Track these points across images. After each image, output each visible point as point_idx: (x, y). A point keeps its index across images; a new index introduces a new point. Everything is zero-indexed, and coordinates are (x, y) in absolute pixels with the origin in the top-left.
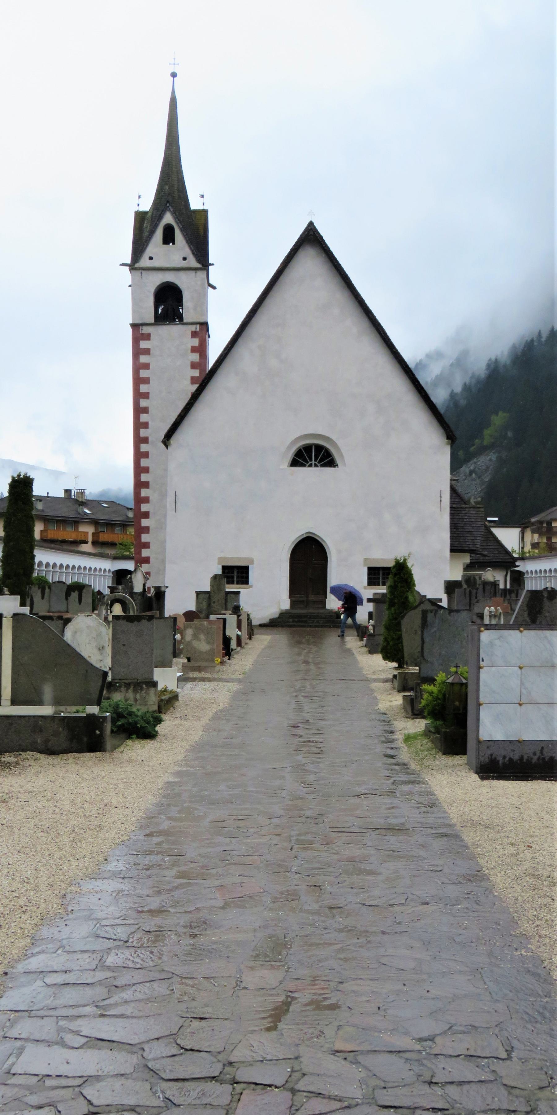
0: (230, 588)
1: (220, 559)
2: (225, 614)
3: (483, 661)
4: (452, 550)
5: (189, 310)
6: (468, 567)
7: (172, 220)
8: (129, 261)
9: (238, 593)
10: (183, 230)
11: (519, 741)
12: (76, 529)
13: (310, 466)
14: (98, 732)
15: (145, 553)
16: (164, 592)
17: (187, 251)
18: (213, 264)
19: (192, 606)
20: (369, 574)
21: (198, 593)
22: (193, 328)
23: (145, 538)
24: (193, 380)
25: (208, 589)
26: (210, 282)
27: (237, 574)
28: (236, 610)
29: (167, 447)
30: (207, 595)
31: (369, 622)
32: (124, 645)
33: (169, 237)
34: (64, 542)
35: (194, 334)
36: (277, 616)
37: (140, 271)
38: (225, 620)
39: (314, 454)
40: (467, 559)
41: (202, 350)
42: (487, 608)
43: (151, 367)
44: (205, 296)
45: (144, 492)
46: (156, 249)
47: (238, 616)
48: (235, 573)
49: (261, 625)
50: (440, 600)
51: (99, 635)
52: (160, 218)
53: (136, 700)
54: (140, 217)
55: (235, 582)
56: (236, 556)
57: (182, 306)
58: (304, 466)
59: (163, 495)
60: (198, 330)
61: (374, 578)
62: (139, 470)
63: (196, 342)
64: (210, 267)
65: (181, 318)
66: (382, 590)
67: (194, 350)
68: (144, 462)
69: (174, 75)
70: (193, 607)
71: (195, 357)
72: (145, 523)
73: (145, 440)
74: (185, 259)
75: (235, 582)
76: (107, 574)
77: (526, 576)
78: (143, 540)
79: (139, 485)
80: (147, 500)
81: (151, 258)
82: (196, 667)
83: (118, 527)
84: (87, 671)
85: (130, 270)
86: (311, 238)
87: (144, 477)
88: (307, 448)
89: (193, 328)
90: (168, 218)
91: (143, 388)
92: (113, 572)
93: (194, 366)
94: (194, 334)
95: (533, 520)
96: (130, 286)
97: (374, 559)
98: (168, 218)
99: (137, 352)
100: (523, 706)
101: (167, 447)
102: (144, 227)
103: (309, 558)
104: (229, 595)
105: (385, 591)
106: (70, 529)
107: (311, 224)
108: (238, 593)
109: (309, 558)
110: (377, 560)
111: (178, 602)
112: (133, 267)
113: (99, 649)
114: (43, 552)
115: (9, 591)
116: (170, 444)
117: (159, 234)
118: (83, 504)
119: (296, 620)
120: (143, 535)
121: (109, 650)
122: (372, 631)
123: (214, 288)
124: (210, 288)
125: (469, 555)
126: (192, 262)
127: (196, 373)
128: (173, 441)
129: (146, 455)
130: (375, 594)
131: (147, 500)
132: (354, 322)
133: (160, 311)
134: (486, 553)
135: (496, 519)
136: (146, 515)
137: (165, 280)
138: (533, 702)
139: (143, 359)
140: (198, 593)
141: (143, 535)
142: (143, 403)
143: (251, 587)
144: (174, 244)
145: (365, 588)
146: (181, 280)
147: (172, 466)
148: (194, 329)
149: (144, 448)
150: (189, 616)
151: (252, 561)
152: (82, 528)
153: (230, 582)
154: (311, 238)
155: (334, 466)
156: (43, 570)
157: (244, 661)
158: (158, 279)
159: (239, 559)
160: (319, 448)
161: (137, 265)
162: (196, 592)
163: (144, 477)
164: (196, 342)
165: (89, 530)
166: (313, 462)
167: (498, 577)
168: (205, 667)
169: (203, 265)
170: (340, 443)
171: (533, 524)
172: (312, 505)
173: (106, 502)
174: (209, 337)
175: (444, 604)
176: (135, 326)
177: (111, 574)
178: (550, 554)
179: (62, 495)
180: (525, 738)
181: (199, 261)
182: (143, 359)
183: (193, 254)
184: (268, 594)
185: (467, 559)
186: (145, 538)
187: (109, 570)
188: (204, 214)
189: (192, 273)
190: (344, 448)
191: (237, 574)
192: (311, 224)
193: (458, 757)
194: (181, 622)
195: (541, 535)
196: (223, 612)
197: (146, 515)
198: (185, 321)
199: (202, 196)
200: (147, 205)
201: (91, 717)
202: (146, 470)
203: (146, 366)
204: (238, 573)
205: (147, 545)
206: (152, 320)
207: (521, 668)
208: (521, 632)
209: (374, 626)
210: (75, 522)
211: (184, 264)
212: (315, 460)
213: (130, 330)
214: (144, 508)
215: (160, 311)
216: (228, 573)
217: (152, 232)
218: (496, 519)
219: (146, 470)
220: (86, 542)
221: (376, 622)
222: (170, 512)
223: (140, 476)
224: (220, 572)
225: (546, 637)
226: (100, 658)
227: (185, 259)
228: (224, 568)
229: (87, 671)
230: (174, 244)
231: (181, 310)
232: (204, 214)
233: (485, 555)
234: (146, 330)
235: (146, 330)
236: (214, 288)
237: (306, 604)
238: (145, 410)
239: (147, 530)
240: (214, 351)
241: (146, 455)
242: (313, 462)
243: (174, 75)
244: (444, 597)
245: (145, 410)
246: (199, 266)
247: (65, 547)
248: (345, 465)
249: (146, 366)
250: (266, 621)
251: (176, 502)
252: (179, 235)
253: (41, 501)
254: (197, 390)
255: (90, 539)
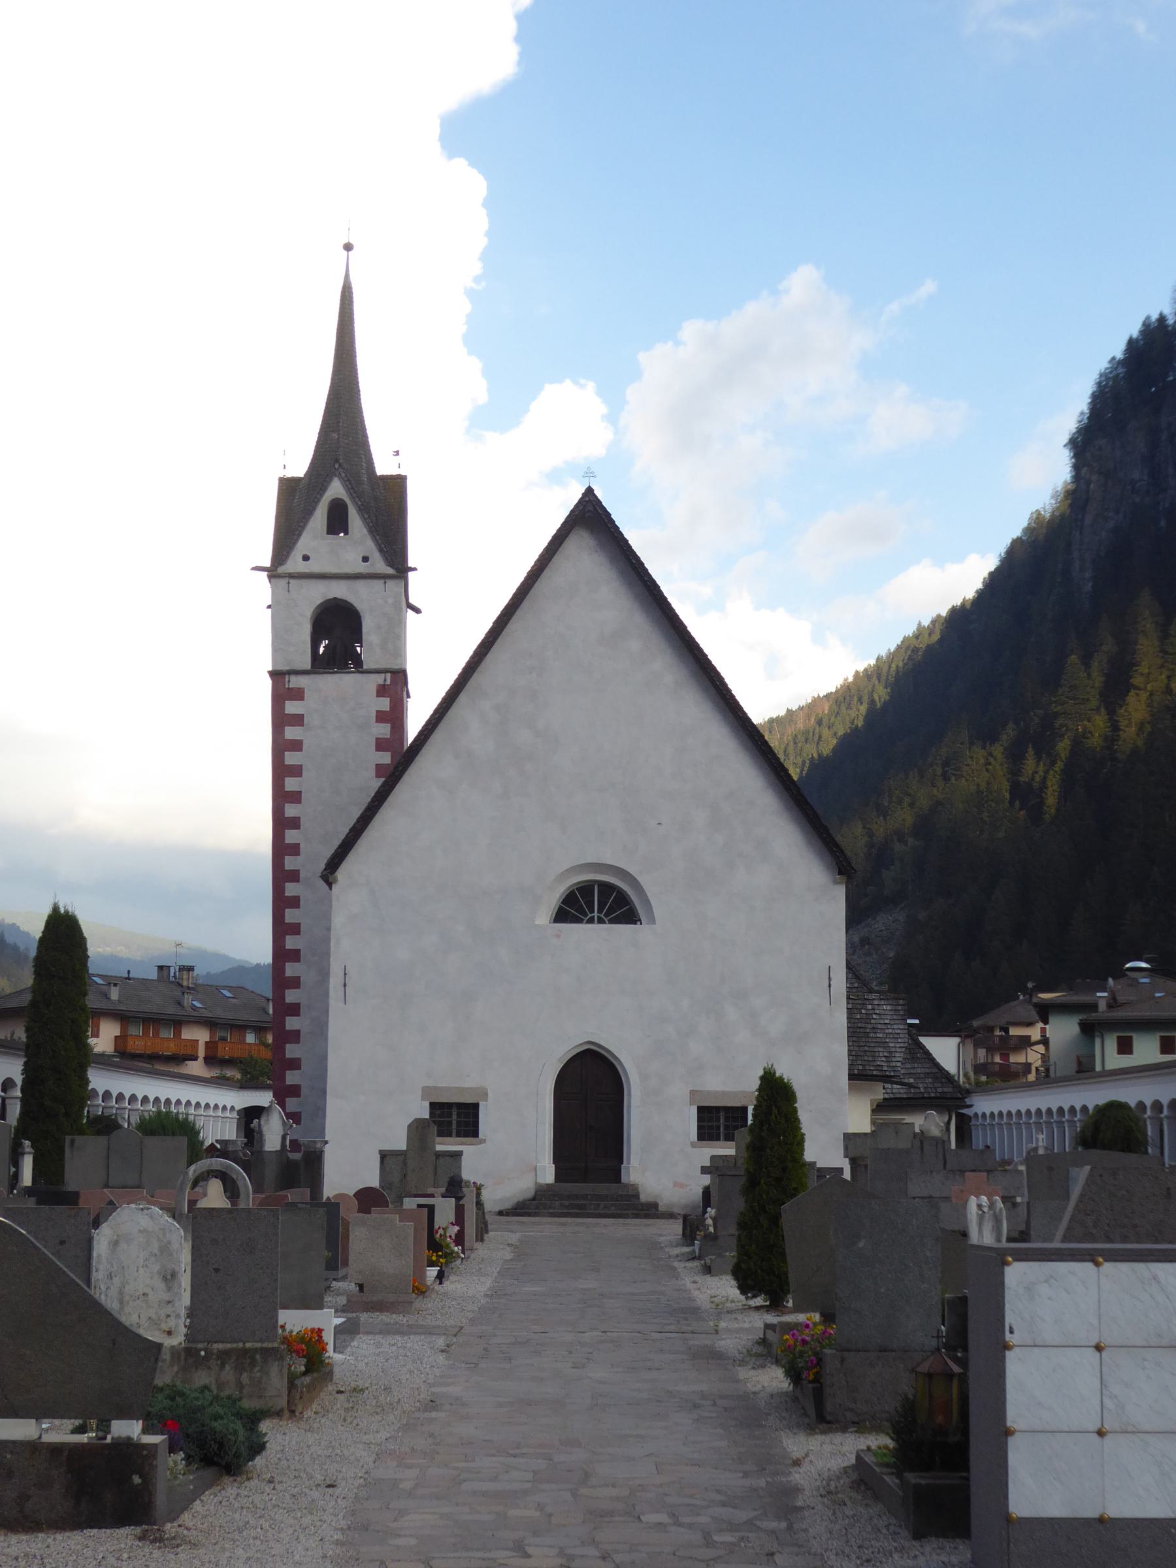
0: (444, 1145)
1: (426, 1091)
2: (432, 1196)
3: (1011, 1332)
4: (852, 1077)
5: (370, 651)
6: (879, 1108)
7: (345, 503)
8: (267, 563)
9: (459, 1154)
10: (362, 510)
11: (1101, 1520)
12: (178, 1034)
13: (591, 921)
14: (137, 1480)
15: (291, 1078)
16: (322, 1152)
17: (369, 546)
18: (414, 569)
19: (372, 1179)
20: (700, 1119)
21: (384, 1156)
22: (379, 679)
23: (291, 1051)
24: (379, 768)
25: (403, 1146)
26: (411, 601)
27: (457, 1117)
28: (455, 1187)
29: (330, 885)
30: (401, 1158)
31: (705, 1212)
32: (217, 1270)
33: (337, 522)
34: (154, 1058)
35: (382, 691)
36: (531, 1194)
37: (287, 580)
38: (431, 1209)
39: (600, 900)
40: (879, 1092)
41: (395, 716)
42: (973, 1198)
43: (305, 747)
44: (401, 623)
45: (291, 970)
46: (313, 535)
47: (458, 1199)
48: (454, 1117)
49: (500, 1213)
50: (841, 1170)
51: (165, 1249)
52: (323, 489)
53: (240, 1386)
54: (288, 487)
55: (454, 1131)
56: (457, 1081)
57: (360, 641)
58: (579, 921)
59: (324, 974)
60: (388, 682)
61: (711, 1128)
62: (282, 929)
63: (385, 704)
64: (411, 574)
65: (358, 662)
66: (727, 1150)
67: (381, 717)
68: (291, 916)
69: (348, 247)
70: (374, 1181)
71: (384, 730)
72: (291, 1023)
73: (294, 876)
74: (365, 559)
75: (454, 1131)
76: (228, 1114)
77: (973, 1122)
78: (288, 1055)
79: (282, 955)
80: (295, 983)
81: (306, 558)
82: (372, 1301)
83: (262, 1030)
84: (114, 1342)
85: (270, 577)
86: (590, 518)
87: (291, 942)
88: (585, 889)
89: (379, 679)
90: (336, 489)
91: (291, 784)
92: (239, 1112)
93: (381, 745)
94: (382, 691)
95: (976, 1023)
96: (269, 607)
97: (708, 1092)
98: (336, 489)
99: (281, 720)
100: (1108, 1439)
101: (330, 885)
102: (295, 501)
103: (590, 1094)
104: (441, 1160)
105: (732, 1152)
106: (167, 1033)
107: (589, 491)
108: (459, 1154)
109: (590, 1094)
110: (716, 1094)
111: (348, 1169)
112: (274, 572)
113: (165, 1279)
114: (108, 1074)
115: (32, 1147)
116: (336, 881)
117: (320, 517)
118: (192, 990)
119: (567, 1203)
120: (288, 1046)
121: (185, 1281)
122: (711, 1229)
123: (417, 611)
124: (410, 612)
125: (881, 1084)
126: (379, 565)
127: (386, 758)
128: (341, 874)
129: (295, 902)
130: (713, 1158)
131: (295, 983)
132: (664, 665)
133: (322, 650)
134: (912, 1080)
135: (917, 1022)
136: (294, 1010)
137: (331, 596)
138: (1130, 1429)
139: (291, 733)
140: (384, 1156)
141: (288, 1046)
142: (291, 811)
143: (484, 1141)
144: (346, 533)
145: (693, 1145)
146: (360, 596)
147: (338, 920)
148: (381, 682)
149: (291, 889)
150: (367, 1199)
151: (485, 1095)
152: (188, 1034)
153: (444, 1132)
154: (590, 518)
155: (635, 923)
156: (98, 1106)
157: (468, 1285)
158: (317, 594)
159: (462, 1090)
160: (607, 889)
161: (281, 570)
162: (381, 1152)
163: (291, 942)
164: (385, 704)
165: (201, 1036)
166: (596, 914)
167: (928, 1122)
168: (392, 1303)
169: (397, 570)
170: (643, 880)
171: (976, 1031)
172: (599, 991)
173: (229, 988)
174: (408, 696)
175: (847, 1175)
176: (275, 675)
177: (235, 1115)
178: (1003, 1084)
179: (153, 975)
180: (1115, 1510)
181: (390, 563)
182: (291, 733)
183: (381, 551)
184: (515, 1150)
185: (879, 1092)
186: (291, 1051)
187: (232, 1108)
188: (397, 485)
189: (378, 584)
190: (656, 889)
191: (457, 1117)
192: (589, 491)
193: (948, 1544)
194: (349, 1212)
195: (990, 1050)
196: (430, 1190)
197: (294, 1010)
198: (365, 667)
199: (397, 453)
200: (299, 468)
201: (126, 1446)
202: (295, 929)
203: (297, 746)
204: (459, 1115)
205: (295, 1064)
206: (307, 665)
207: (1099, 1348)
208: (1097, 1264)
209: (714, 1219)
210: (178, 1023)
211: (363, 568)
212: (600, 911)
213: (268, 683)
214: (291, 996)
215: (322, 650)
216: (439, 1116)
217: (309, 512)
218: (917, 1022)
219: (295, 929)
220: (196, 1059)
221: (718, 1210)
222: (335, 1003)
223: (284, 941)
224: (426, 1115)
225: (1155, 1278)
226: (166, 1296)
227: (365, 559)
228: (433, 1106)
229: (114, 1342)
230: (346, 533)
231: (358, 649)
232: (397, 485)
233: (910, 1085)
234: (295, 682)
235: (295, 682)
236: (417, 611)
237: (583, 1176)
238: (295, 823)
239: (295, 1036)
240: (415, 720)
241: (295, 902)
242: (596, 914)
243: (348, 247)
244: (846, 1165)
245: (295, 823)
246: (390, 571)
247: (159, 1067)
248: (652, 920)
249: (297, 746)
250: (507, 1205)
251: (345, 985)
252: (355, 520)
253: (115, 985)
254: (383, 785)
255: (201, 1053)
